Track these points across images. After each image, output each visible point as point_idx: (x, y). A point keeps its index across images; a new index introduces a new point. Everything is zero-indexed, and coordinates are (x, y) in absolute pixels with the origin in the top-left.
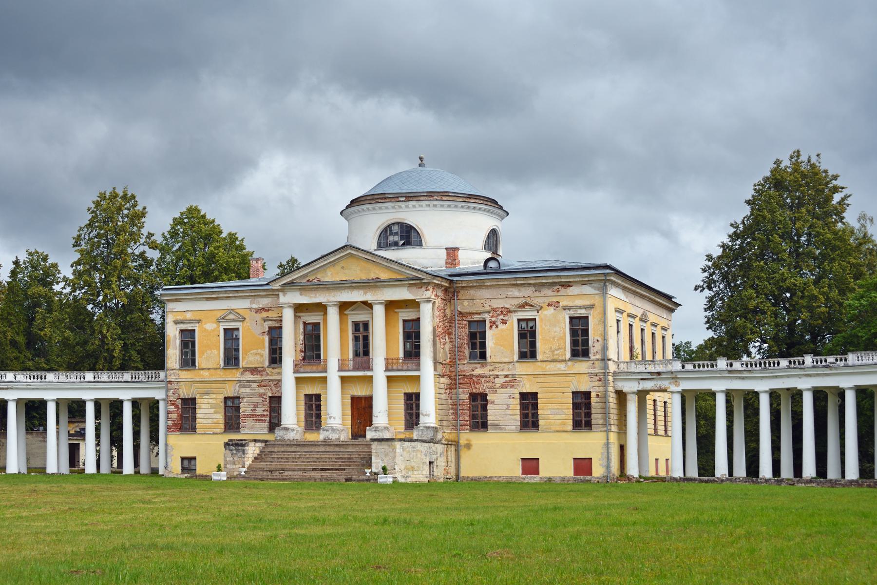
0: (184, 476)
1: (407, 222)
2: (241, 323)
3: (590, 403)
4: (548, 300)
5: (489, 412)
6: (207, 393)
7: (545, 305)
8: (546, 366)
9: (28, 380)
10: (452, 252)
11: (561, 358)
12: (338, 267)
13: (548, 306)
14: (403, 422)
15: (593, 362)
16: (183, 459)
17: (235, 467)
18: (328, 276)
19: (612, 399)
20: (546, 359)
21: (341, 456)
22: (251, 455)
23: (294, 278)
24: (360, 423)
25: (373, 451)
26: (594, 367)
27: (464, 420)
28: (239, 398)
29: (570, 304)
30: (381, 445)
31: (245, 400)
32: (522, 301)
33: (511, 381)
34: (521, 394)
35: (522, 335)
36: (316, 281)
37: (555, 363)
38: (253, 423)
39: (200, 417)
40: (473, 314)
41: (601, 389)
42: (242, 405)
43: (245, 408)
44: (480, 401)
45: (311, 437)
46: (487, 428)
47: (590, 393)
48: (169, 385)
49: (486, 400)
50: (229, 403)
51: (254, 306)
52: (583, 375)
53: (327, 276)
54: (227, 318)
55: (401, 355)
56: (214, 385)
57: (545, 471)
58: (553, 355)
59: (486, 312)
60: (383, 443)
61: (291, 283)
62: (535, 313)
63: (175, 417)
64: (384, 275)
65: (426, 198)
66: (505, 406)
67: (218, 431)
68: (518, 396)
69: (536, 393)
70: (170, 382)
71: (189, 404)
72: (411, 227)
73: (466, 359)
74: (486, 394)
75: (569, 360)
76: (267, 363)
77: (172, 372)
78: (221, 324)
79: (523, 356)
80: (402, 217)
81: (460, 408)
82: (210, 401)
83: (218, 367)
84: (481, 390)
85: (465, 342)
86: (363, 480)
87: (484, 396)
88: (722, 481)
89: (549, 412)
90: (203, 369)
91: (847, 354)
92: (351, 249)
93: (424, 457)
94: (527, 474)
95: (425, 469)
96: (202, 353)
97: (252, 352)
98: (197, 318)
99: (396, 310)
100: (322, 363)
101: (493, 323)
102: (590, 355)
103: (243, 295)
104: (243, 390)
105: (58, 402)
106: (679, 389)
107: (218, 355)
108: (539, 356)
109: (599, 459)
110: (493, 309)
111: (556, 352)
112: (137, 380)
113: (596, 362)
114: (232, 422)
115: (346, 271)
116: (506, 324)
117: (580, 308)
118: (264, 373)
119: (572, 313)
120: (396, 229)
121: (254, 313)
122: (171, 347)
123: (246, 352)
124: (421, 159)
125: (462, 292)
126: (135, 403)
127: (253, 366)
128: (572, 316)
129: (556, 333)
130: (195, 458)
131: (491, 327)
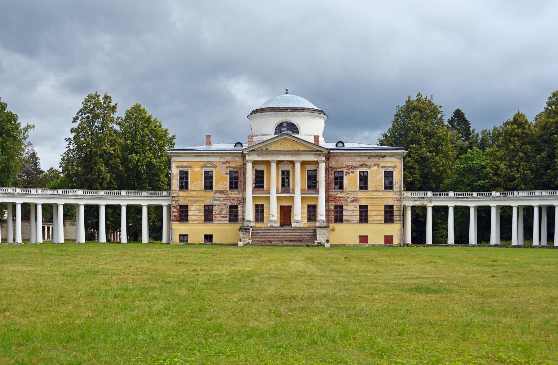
0: (180, 244)
1: (292, 122)
2: (214, 169)
3: (393, 210)
4: (374, 163)
6: (195, 203)
7: (373, 165)
9: (108, 194)
11: (380, 190)
12: (278, 144)
13: (374, 165)
14: (306, 218)
16: (180, 235)
17: (245, 240)
18: (273, 148)
21: (295, 235)
23: (255, 148)
24: (285, 219)
26: (396, 195)
27: (331, 218)
28: (212, 206)
29: (385, 165)
31: (216, 207)
32: (362, 163)
33: (355, 200)
34: (359, 206)
35: (361, 179)
37: (377, 192)
38: (220, 218)
40: (337, 168)
41: (399, 204)
42: (214, 209)
43: (216, 210)
45: (259, 225)
47: (393, 206)
48: (173, 198)
50: (207, 208)
51: (222, 160)
52: (390, 198)
53: (272, 148)
54: (206, 166)
55: (306, 187)
56: (199, 199)
57: (370, 242)
60: (323, 228)
61: (253, 150)
62: (368, 169)
64: (302, 149)
65: (301, 111)
66: (352, 212)
67: (201, 222)
68: (358, 207)
69: (367, 206)
70: (174, 197)
72: (293, 124)
74: (343, 206)
75: (384, 191)
76: (228, 189)
77: (175, 192)
78: (203, 169)
79: (361, 188)
80: (289, 119)
82: (196, 207)
83: (201, 190)
84: (340, 204)
85: (333, 181)
86: (313, 246)
87: (341, 207)
88: (452, 246)
89: (373, 215)
90: (192, 191)
91: (513, 191)
92: (286, 135)
94: (362, 243)
97: (220, 183)
98: (189, 165)
99: (305, 165)
101: (347, 173)
102: (394, 189)
103: (217, 154)
104: (215, 202)
105: (518, 207)
106: (432, 205)
108: (369, 189)
109: (397, 236)
110: (347, 166)
111: (378, 187)
112: (139, 195)
113: (397, 192)
115: (282, 146)
116: (353, 173)
117: (390, 167)
118: (227, 193)
119: (386, 169)
120: (285, 125)
121: (222, 164)
122: (174, 179)
123: (217, 183)
124: (287, 90)
125: (332, 158)
127: (221, 190)
130: (187, 235)
131: (346, 175)
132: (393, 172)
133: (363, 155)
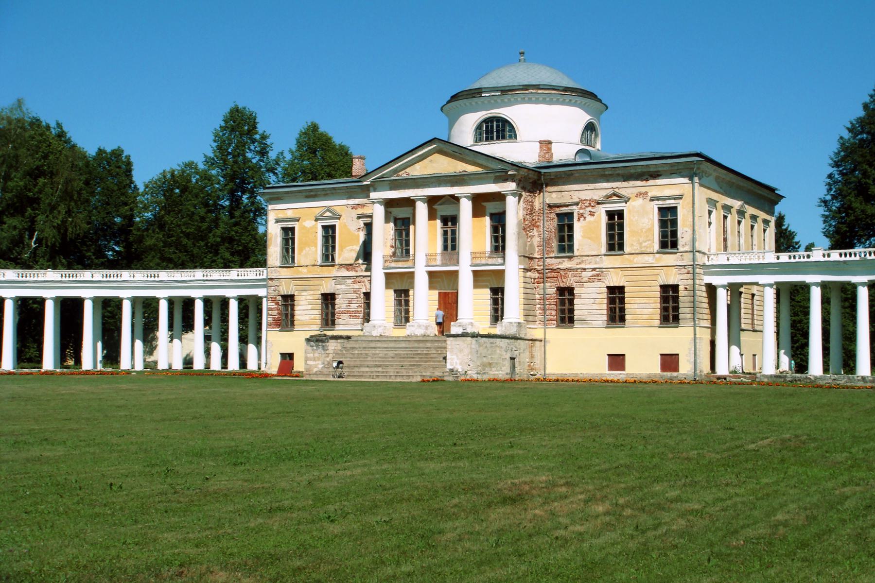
5: (576, 307)
8: (634, 258)
10: (546, 144)
11: (648, 251)
13: (637, 196)
15: (681, 254)
18: (417, 171)
19: (702, 295)
20: (633, 252)
21: (419, 352)
22: (332, 352)
25: (449, 347)
27: (551, 315)
29: (659, 194)
30: (456, 341)
33: (598, 275)
34: (608, 288)
36: (405, 175)
39: (630, 307)
43: (340, 303)
44: (566, 295)
46: (624, 322)
49: (573, 295)
58: (641, 247)
59: (574, 205)
63: (275, 314)
64: (471, 169)
71: (289, 300)
73: (553, 252)
81: (547, 303)
84: (568, 285)
87: (571, 290)
93: (505, 353)
95: (505, 365)
96: (301, 250)
97: (348, 248)
100: (411, 258)
102: (678, 247)
104: (339, 286)
107: (317, 251)
108: (627, 249)
110: (582, 201)
111: (644, 244)
114: (329, 318)
116: (593, 216)
126: (207, 301)
128: (661, 206)
129: (644, 225)
131: (579, 219)
132: (676, 208)
133: (610, 175)
